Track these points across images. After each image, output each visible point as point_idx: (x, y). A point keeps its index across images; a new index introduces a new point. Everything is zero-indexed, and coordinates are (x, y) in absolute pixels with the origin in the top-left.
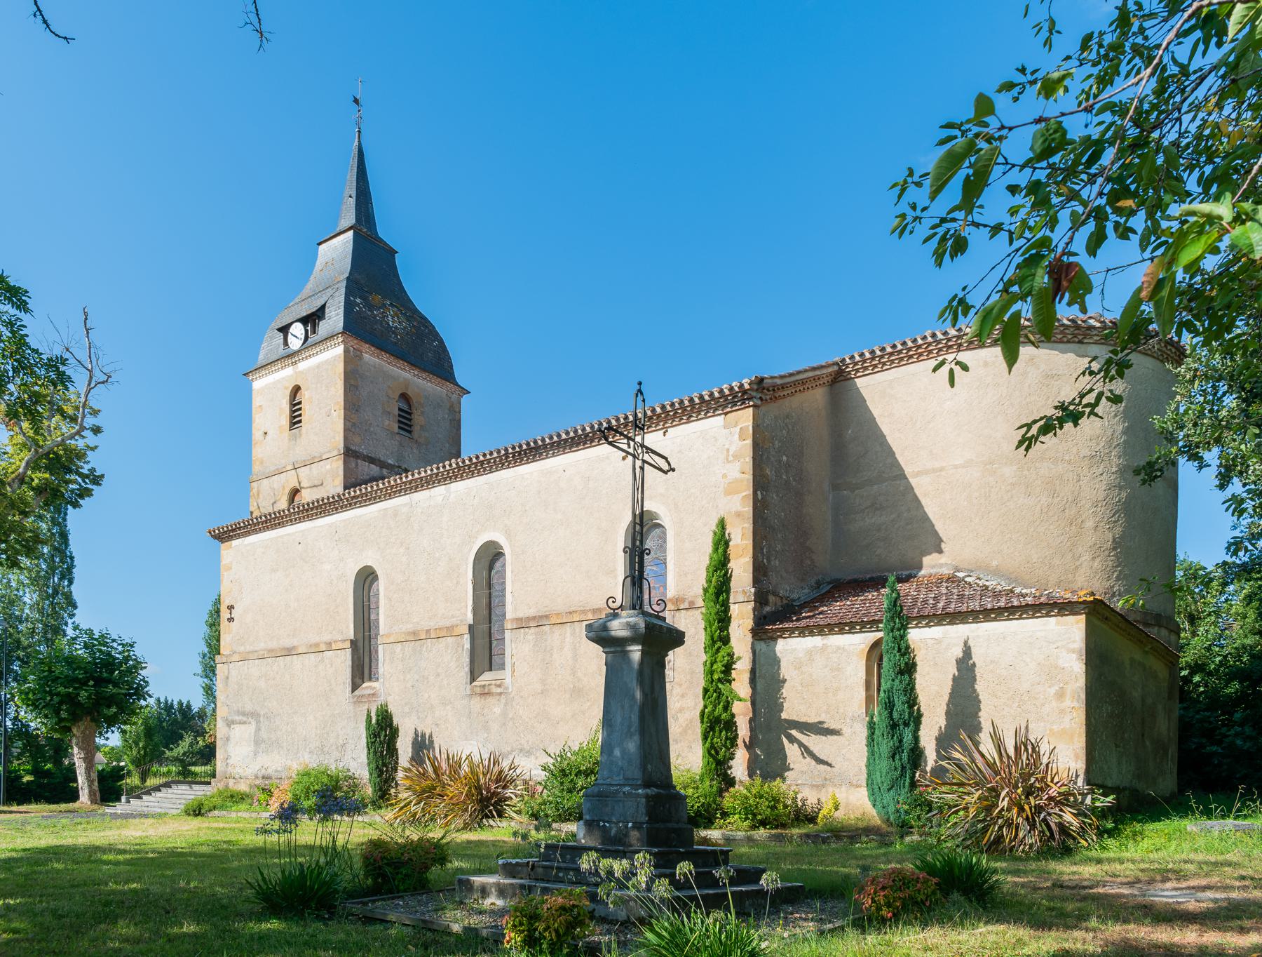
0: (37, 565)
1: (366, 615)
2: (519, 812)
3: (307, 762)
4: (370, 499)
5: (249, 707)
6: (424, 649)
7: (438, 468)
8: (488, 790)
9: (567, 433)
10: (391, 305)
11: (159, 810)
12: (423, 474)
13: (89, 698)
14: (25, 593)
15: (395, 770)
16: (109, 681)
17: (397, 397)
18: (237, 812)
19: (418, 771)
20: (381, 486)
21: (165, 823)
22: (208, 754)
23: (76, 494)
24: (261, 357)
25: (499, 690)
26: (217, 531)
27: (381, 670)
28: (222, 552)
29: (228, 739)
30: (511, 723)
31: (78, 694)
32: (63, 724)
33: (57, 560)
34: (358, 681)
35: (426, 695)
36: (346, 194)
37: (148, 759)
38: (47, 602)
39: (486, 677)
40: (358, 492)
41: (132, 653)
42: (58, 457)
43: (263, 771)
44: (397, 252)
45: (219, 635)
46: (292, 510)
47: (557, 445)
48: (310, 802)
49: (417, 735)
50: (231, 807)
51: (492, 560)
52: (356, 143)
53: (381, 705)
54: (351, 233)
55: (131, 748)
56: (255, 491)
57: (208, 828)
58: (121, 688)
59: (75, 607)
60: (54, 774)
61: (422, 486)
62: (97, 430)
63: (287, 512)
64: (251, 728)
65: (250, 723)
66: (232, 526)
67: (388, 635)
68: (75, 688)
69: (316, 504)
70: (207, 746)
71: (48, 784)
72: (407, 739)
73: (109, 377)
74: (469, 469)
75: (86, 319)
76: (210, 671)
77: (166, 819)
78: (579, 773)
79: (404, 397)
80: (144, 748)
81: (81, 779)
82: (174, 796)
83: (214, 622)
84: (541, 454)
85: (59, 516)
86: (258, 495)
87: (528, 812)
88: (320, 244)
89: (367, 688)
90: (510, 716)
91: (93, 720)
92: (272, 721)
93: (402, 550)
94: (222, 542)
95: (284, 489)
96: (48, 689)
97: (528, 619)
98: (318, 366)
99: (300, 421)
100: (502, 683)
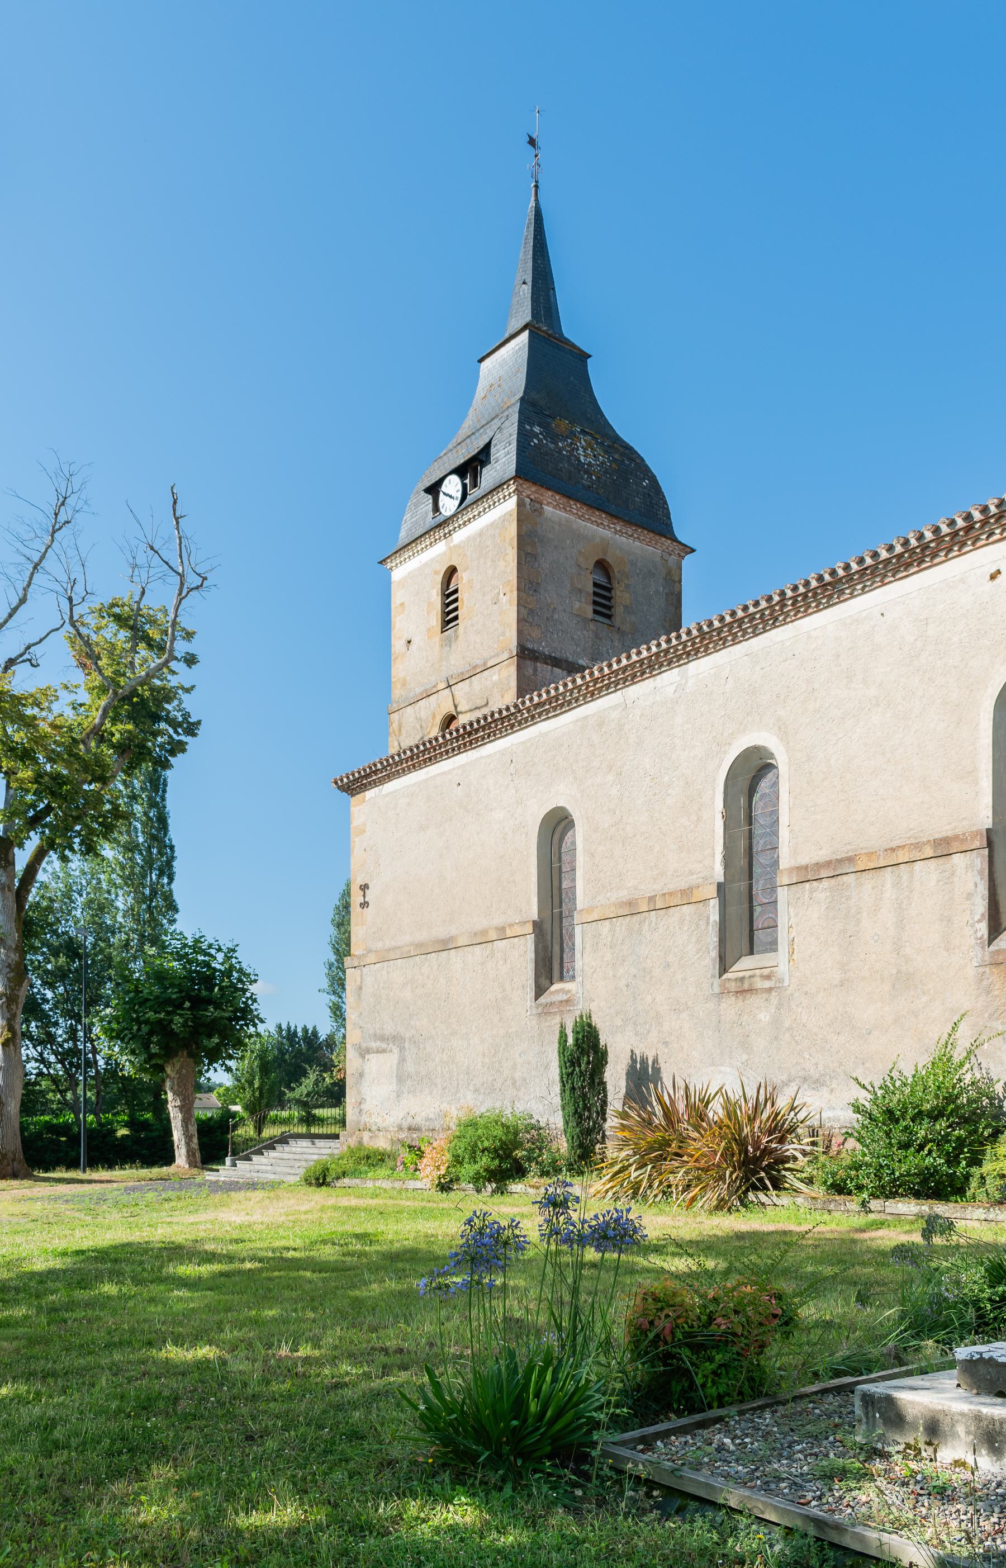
0: (130, 859)
1: (556, 883)
2: (810, 1181)
3: (471, 1104)
4: (562, 705)
5: (389, 1029)
6: (646, 927)
7: (669, 641)
8: (756, 1145)
9: (890, 548)
10: (583, 432)
11: (272, 1177)
12: (645, 654)
13: (185, 1025)
14: (117, 896)
15: (603, 1113)
16: (209, 1001)
17: (591, 567)
18: (375, 1179)
19: (639, 1116)
20: (579, 681)
21: (278, 1197)
22: (336, 1095)
23: (167, 751)
24: (403, 534)
25: (767, 984)
26: (345, 780)
27: (578, 964)
28: (352, 809)
29: (361, 1075)
30: (787, 1035)
31: (171, 1021)
32: (154, 1062)
33: (155, 851)
34: (544, 982)
35: (649, 998)
36: (519, 280)
37: (264, 1101)
38: (144, 906)
39: (746, 964)
40: (544, 696)
41: (234, 961)
42: (143, 701)
43: (410, 1119)
44: (590, 356)
45: (349, 937)
46: (448, 736)
47: (872, 573)
48: (477, 1167)
49: (634, 1060)
50: (366, 1172)
51: (754, 777)
52: (532, 204)
53: (581, 1017)
54: (525, 335)
55: (244, 1090)
56: (395, 725)
57: (336, 1208)
58: (224, 1010)
59: (177, 911)
60: (152, 1125)
61: (643, 673)
62: (191, 660)
63: (441, 740)
64: (393, 1058)
65: (391, 1051)
66: (365, 770)
67: (590, 910)
68: (168, 1013)
69: (482, 722)
70: (334, 1084)
71: (146, 1139)
72: (619, 1068)
73: (205, 579)
74: (719, 634)
75: (175, 502)
76: (339, 985)
77: (279, 1192)
78: (919, 1116)
79: (602, 566)
80: (260, 1088)
81: (177, 1135)
82: (291, 1156)
83: (342, 921)
84: (842, 592)
85: (157, 794)
86: (400, 730)
87: (825, 1182)
88: (481, 361)
89: (557, 991)
90: (787, 1024)
91: (191, 1055)
92: (421, 1046)
93: (610, 778)
94: (353, 795)
95: (434, 716)
96: (135, 1016)
97: (818, 866)
98: (481, 534)
99: (456, 618)
100: (772, 972)
